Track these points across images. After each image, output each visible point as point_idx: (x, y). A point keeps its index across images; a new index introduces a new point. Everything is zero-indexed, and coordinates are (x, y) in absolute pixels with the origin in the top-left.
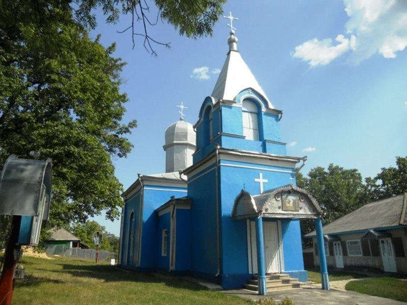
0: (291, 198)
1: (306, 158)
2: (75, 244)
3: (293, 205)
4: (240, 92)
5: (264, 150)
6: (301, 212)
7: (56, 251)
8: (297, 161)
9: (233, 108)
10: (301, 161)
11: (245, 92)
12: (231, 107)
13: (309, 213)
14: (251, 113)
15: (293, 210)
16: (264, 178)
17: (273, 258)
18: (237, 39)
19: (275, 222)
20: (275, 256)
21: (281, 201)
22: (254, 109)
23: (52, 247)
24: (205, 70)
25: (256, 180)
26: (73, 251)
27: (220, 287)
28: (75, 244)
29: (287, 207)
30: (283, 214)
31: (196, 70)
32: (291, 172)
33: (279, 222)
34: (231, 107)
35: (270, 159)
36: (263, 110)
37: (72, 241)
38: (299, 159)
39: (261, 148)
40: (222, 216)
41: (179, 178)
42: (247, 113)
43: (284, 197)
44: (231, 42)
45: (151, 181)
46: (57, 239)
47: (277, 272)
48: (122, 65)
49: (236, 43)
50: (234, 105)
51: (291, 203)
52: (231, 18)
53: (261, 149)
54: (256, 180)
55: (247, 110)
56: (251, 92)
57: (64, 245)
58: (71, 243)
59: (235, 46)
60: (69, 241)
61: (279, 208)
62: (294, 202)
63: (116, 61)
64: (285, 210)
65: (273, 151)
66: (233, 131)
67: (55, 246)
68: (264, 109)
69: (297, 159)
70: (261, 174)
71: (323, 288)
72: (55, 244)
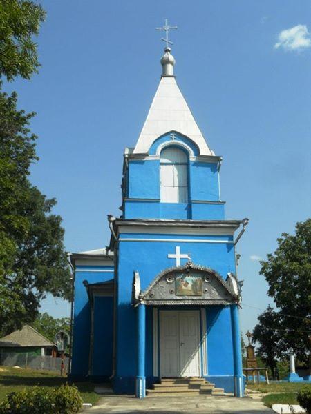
0: (190, 279)
1: (246, 221)
2: (49, 350)
3: (193, 288)
4: (155, 142)
5: (190, 216)
6: (207, 297)
7: (18, 361)
8: (236, 225)
9: (145, 163)
10: (241, 225)
11: (164, 138)
12: (142, 162)
13: (218, 298)
14: (176, 164)
15: (193, 294)
16: (182, 252)
17: (192, 359)
18: (171, 58)
19: (199, 311)
20: (195, 355)
21: (174, 285)
22: (180, 159)
23: (12, 356)
24: (301, 30)
25: (170, 256)
26: (48, 360)
27: (111, 391)
28: (49, 350)
29: (182, 290)
30: (177, 300)
31: (285, 35)
32: (227, 241)
33: (204, 311)
34: (142, 162)
35: (193, 227)
36: (191, 159)
37: (44, 347)
38: (238, 223)
39: (186, 211)
40: (119, 303)
41: (105, 253)
42: (171, 166)
43: (179, 278)
44: (165, 63)
45: (85, 260)
46: (22, 345)
47: (198, 376)
48: (29, 116)
49: (172, 63)
50: (147, 159)
51: (190, 285)
52: (167, 27)
53: (185, 214)
54: (170, 256)
55: (170, 162)
56: (173, 137)
57: (34, 354)
58: (43, 350)
59: (170, 69)
60: (40, 347)
61: (171, 292)
62: (195, 284)
63: (19, 114)
64: (178, 295)
65: (200, 215)
66: (144, 194)
67: (17, 355)
68: (193, 158)
69: (235, 224)
70: (178, 248)
71: (235, 396)
72: (17, 352)
